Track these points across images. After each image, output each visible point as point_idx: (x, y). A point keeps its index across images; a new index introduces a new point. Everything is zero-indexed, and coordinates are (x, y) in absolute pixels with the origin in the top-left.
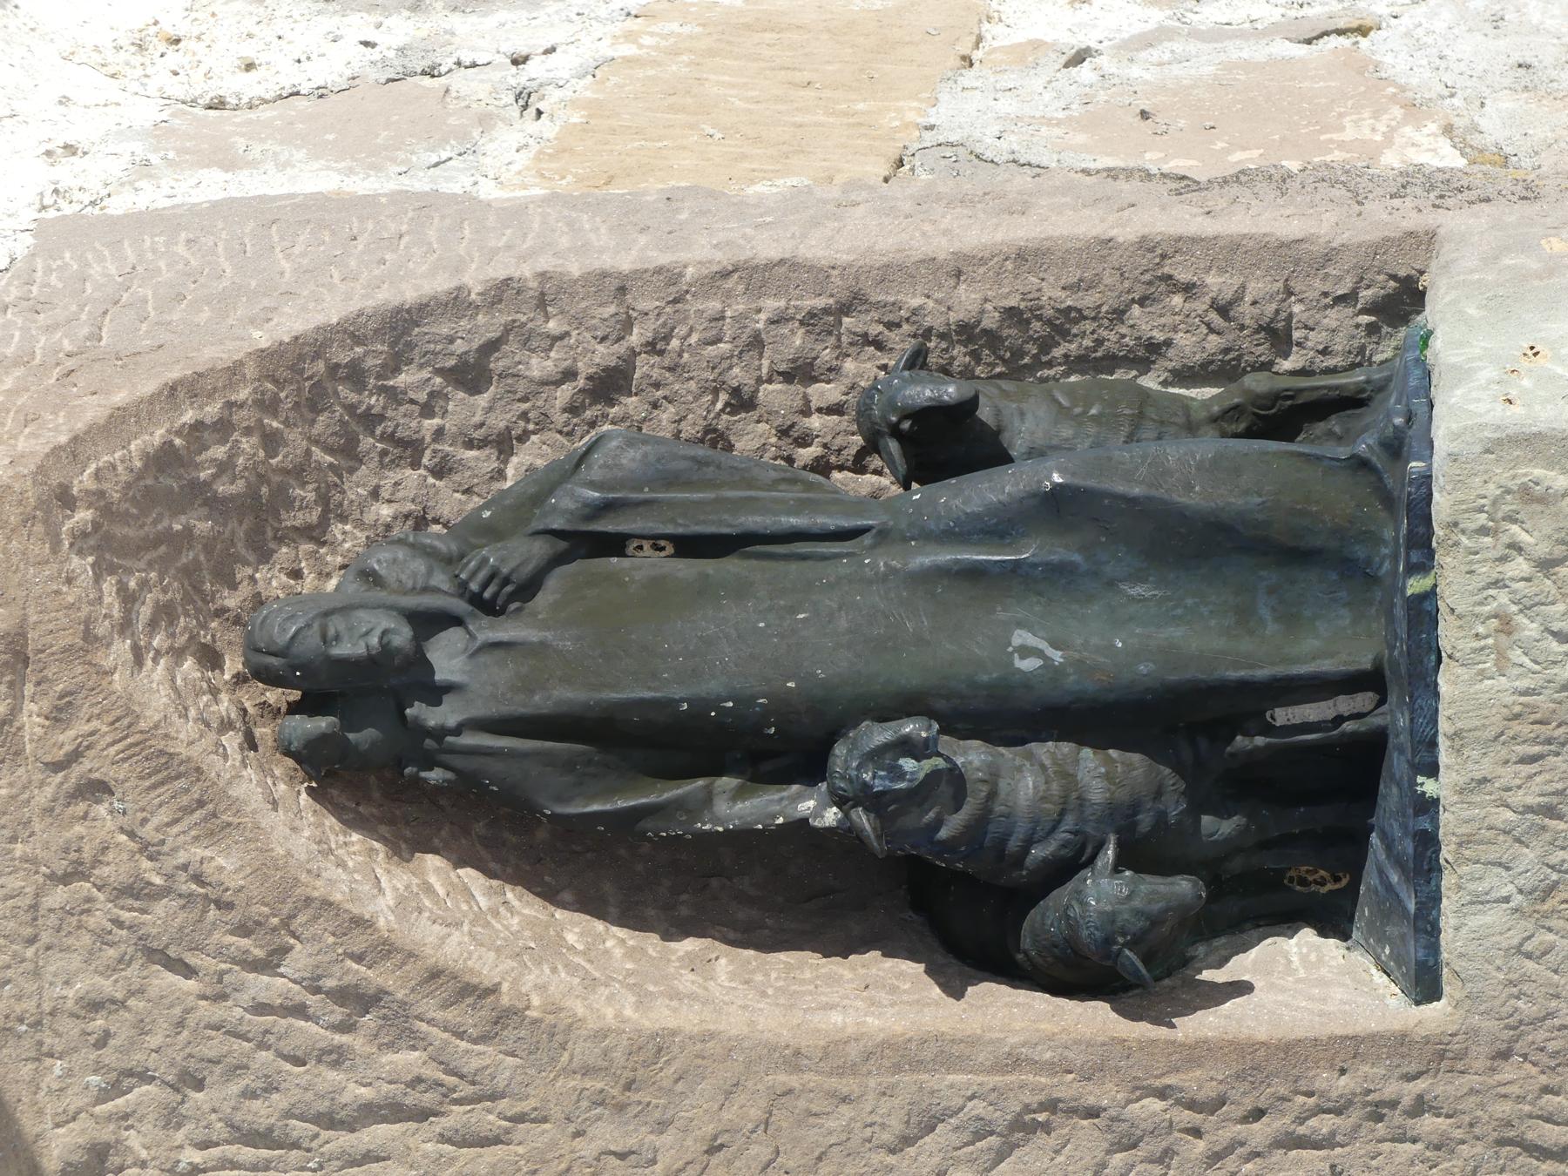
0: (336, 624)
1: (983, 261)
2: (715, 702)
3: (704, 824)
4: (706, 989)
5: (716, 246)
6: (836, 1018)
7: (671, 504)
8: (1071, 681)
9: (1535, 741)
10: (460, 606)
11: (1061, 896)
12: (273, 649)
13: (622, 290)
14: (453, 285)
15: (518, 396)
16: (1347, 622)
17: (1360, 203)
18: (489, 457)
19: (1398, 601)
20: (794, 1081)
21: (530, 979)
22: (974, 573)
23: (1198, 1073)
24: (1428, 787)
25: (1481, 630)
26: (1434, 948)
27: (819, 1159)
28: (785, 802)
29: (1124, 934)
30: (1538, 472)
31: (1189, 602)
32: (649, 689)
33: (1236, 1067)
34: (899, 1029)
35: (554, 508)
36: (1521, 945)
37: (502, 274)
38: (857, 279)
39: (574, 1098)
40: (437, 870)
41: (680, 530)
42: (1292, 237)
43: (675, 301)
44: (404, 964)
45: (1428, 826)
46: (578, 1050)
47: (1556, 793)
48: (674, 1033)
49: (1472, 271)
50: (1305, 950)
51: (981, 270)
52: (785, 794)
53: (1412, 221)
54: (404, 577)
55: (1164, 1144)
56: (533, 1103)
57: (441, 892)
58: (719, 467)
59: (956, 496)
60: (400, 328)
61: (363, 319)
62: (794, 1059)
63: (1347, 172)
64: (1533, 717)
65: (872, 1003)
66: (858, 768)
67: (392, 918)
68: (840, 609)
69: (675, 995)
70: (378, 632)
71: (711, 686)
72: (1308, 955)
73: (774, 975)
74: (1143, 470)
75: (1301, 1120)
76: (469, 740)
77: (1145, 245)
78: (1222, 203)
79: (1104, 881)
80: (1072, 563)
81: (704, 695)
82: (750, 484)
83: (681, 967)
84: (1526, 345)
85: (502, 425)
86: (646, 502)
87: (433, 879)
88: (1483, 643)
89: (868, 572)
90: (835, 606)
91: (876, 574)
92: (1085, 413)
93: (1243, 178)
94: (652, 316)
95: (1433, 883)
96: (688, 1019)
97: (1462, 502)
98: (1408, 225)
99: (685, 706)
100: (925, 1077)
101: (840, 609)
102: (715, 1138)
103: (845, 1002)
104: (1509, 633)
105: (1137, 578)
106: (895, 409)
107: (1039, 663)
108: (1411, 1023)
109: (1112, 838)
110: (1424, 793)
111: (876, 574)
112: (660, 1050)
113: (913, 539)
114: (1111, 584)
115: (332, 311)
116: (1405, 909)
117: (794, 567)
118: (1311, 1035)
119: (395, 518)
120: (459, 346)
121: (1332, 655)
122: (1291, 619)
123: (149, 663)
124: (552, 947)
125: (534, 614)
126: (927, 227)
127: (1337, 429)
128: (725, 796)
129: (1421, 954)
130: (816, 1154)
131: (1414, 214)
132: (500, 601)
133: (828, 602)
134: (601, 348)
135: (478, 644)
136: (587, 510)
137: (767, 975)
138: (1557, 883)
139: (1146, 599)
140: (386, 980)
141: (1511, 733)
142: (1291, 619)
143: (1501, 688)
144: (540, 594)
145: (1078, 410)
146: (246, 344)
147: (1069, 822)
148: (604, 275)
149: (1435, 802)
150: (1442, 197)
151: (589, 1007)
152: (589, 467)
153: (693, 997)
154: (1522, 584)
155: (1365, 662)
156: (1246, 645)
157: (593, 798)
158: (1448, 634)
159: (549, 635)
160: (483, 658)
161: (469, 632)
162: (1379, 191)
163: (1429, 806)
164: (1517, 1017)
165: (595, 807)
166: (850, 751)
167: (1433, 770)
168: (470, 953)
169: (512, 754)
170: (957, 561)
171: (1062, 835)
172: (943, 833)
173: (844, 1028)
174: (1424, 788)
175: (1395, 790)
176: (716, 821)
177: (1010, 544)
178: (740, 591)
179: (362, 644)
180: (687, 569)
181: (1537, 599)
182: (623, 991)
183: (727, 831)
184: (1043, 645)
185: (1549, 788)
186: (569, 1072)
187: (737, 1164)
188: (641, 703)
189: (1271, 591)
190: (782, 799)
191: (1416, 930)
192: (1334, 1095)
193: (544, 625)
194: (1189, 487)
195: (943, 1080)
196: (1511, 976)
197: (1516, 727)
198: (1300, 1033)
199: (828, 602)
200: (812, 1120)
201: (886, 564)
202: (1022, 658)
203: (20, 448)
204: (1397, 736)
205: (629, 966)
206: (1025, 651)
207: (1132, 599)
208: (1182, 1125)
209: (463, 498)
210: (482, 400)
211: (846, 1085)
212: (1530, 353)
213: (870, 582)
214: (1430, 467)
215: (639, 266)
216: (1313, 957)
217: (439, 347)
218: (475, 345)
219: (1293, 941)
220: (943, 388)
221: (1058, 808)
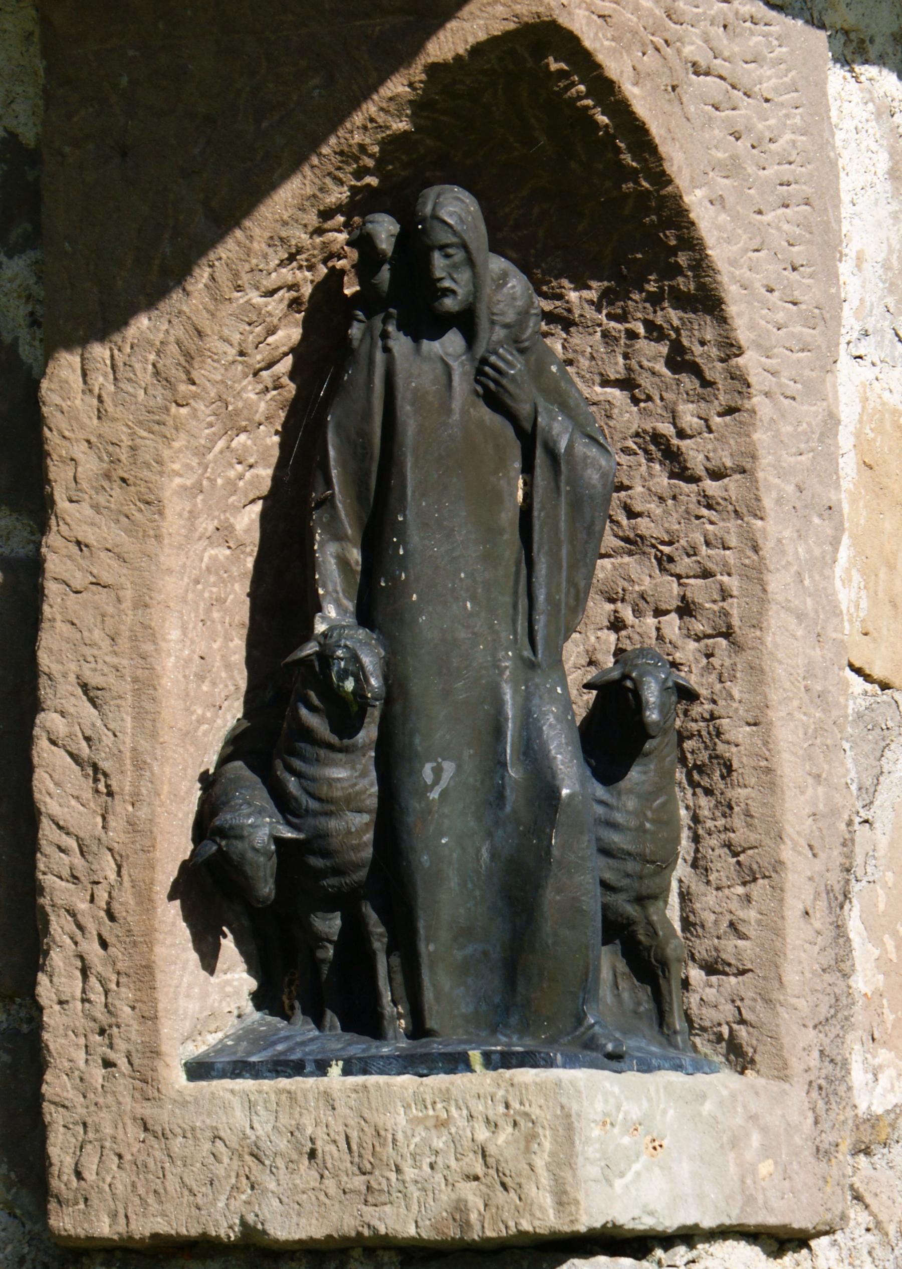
0: (459, 255)
1: (766, 743)
2: (403, 542)
3: (320, 535)
4: (200, 539)
5: (779, 541)
6: (174, 634)
7: (556, 507)
8: (415, 805)
9: (360, 1146)
10: (481, 349)
11: (262, 797)
12: (437, 208)
13: (744, 471)
14: (743, 343)
15: (664, 394)
16: (464, 1010)
17: (815, 1027)
18: (618, 373)
19: (467, 1047)
20: (127, 604)
21: (201, 406)
22: (498, 732)
23: (132, 902)
24: (335, 1070)
25: (439, 1106)
26: (223, 1075)
27: (73, 624)
28: (334, 595)
29: (227, 845)
30: (547, 1145)
31: (477, 893)
32: (414, 492)
33: (136, 929)
34: (164, 681)
35: (554, 419)
36: (220, 1138)
37: (752, 380)
38: (753, 648)
39: (115, 441)
40: (289, 337)
41: (536, 513)
42: (783, 974)
43: (736, 511)
44: (208, 311)
45: (308, 1069)
46: (147, 442)
47: (324, 1161)
48: (161, 513)
49: (745, 1107)
50: (235, 983)
51: (759, 742)
52: (341, 595)
53: (796, 1066)
54: (501, 306)
55: (82, 878)
56: (111, 409)
57: (270, 340)
58: (586, 542)
59: (557, 719)
60: (708, 302)
61: (711, 273)
62: (142, 604)
63: (846, 1019)
64: (377, 1144)
65: (188, 661)
66: (346, 646)
67: (241, 301)
68: (473, 633)
69: (193, 515)
70: (453, 286)
71: (415, 538)
72: (231, 985)
73: (215, 590)
74: (572, 857)
75: (102, 982)
76: (379, 356)
77: (778, 865)
78: (818, 925)
79: (267, 830)
80: (504, 805)
81: (409, 532)
82: (573, 567)
83: (220, 520)
84: (665, 1143)
85: (642, 382)
86: (558, 488)
87: (280, 333)
88: (429, 1106)
89: (501, 654)
90: (476, 630)
91: (500, 660)
92: (648, 820)
93: (841, 941)
94: (725, 494)
95: (268, 1074)
96: (173, 522)
97: (527, 1089)
98: (793, 1062)
99: (400, 519)
100: (130, 702)
101: (473, 633)
102: (87, 546)
103: (188, 643)
104: (436, 1126)
105: (493, 856)
106: (641, 676)
107: (429, 781)
108: (168, 1059)
109: (302, 836)
110: (330, 1066)
111: (500, 660)
112: (148, 503)
113: (527, 687)
114: (490, 835)
115: (718, 252)
116: (253, 1054)
117: (507, 599)
118: (158, 985)
119: (568, 302)
120: (697, 349)
121: (437, 998)
122: (465, 969)
123: (425, 114)
124: (235, 424)
125: (473, 405)
126: (796, 703)
127: (642, 1009)
128: (340, 550)
129: (219, 1066)
130: (75, 621)
131: (803, 1066)
132: (483, 379)
133: (479, 624)
134: (701, 457)
135: (451, 362)
136: (551, 444)
137: (214, 585)
138: (263, 1164)
139: (478, 861)
140: (196, 298)
141: (366, 1129)
142: (465, 969)
143: (398, 1120)
144: (488, 410)
145: (649, 814)
146: (687, 184)
147: (313, 805)
148: (754, 457)
149: (324, 1074)
150: (820, 1088)
151: (180, 450)
152: (585, 445)
153: (192, 528)
154: (470, 1135)
155: (431, 1023)
156: (444, 935)
157: (338, 451)
158: (438, 1081)
159: (456, 417)
160: (439, 367)
161: (461, 356)
162: (826, 1041)
163: (322, 1068)
164: (170, 1136)
165: (332, 453)
166: (360, 641)
167: (346, 1072)
168: (218, 361)
169: (369, 389)
170: (507, 720)
171: (305, 800)
172: (304, 712)
173: (165, 640)
174: (334, 1067)
175: (340, 1046)
176: (322, 544)
177: (519, 759)
178: (489, 558)
179: (443, 275)
180: (509, 517)
181: (458, 1146)
182: (196, 477)
183: (314, 552)
184: (443, 784)
185: (328, 1157)
186: (133, 435)
187: (69, 562)
188: (404, 487)
189: (485, 953)
190: (337, 592)
191: (235, 1062)
192: (117, 1003)
193: (464, 412)
194: (559, 891)
195: (127, 714)
196: (198, 1131)
197: (369, 1131)
198: (159, 976)
199: (479, 624)
200: (99, 618)
201: (507, 667)
202: (433, 769)
203: (578, 11)
204: (377, 1047)
205: (220, 481)
206: (438, 772)
207: (478, 851)
208: (95, 891)
209: (588, 355)
210: (661, 367)
211: (124, 643)
212: (656, 1144)
213: (494, 656)
214: (557, 1067)
215: (761, 485)
216: (229, 989)
217: (696, 333)
218: (698, 360)
219: (245, 975)
220: (656, 712)
221: (323, 797)
